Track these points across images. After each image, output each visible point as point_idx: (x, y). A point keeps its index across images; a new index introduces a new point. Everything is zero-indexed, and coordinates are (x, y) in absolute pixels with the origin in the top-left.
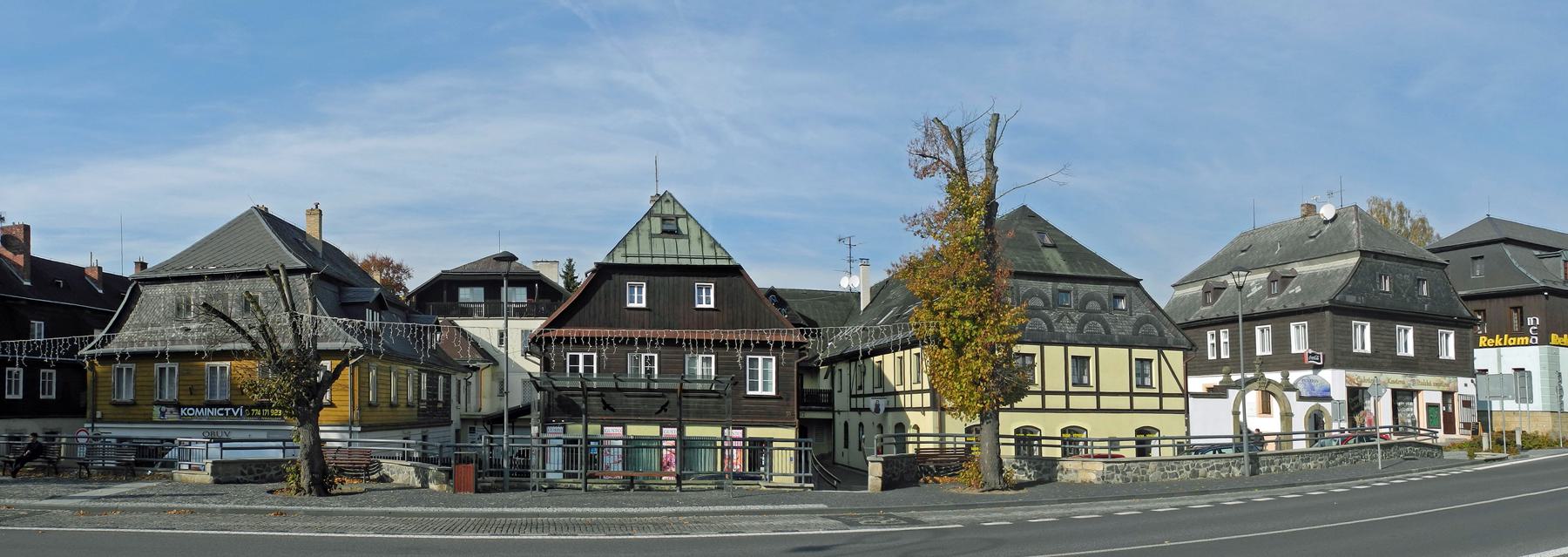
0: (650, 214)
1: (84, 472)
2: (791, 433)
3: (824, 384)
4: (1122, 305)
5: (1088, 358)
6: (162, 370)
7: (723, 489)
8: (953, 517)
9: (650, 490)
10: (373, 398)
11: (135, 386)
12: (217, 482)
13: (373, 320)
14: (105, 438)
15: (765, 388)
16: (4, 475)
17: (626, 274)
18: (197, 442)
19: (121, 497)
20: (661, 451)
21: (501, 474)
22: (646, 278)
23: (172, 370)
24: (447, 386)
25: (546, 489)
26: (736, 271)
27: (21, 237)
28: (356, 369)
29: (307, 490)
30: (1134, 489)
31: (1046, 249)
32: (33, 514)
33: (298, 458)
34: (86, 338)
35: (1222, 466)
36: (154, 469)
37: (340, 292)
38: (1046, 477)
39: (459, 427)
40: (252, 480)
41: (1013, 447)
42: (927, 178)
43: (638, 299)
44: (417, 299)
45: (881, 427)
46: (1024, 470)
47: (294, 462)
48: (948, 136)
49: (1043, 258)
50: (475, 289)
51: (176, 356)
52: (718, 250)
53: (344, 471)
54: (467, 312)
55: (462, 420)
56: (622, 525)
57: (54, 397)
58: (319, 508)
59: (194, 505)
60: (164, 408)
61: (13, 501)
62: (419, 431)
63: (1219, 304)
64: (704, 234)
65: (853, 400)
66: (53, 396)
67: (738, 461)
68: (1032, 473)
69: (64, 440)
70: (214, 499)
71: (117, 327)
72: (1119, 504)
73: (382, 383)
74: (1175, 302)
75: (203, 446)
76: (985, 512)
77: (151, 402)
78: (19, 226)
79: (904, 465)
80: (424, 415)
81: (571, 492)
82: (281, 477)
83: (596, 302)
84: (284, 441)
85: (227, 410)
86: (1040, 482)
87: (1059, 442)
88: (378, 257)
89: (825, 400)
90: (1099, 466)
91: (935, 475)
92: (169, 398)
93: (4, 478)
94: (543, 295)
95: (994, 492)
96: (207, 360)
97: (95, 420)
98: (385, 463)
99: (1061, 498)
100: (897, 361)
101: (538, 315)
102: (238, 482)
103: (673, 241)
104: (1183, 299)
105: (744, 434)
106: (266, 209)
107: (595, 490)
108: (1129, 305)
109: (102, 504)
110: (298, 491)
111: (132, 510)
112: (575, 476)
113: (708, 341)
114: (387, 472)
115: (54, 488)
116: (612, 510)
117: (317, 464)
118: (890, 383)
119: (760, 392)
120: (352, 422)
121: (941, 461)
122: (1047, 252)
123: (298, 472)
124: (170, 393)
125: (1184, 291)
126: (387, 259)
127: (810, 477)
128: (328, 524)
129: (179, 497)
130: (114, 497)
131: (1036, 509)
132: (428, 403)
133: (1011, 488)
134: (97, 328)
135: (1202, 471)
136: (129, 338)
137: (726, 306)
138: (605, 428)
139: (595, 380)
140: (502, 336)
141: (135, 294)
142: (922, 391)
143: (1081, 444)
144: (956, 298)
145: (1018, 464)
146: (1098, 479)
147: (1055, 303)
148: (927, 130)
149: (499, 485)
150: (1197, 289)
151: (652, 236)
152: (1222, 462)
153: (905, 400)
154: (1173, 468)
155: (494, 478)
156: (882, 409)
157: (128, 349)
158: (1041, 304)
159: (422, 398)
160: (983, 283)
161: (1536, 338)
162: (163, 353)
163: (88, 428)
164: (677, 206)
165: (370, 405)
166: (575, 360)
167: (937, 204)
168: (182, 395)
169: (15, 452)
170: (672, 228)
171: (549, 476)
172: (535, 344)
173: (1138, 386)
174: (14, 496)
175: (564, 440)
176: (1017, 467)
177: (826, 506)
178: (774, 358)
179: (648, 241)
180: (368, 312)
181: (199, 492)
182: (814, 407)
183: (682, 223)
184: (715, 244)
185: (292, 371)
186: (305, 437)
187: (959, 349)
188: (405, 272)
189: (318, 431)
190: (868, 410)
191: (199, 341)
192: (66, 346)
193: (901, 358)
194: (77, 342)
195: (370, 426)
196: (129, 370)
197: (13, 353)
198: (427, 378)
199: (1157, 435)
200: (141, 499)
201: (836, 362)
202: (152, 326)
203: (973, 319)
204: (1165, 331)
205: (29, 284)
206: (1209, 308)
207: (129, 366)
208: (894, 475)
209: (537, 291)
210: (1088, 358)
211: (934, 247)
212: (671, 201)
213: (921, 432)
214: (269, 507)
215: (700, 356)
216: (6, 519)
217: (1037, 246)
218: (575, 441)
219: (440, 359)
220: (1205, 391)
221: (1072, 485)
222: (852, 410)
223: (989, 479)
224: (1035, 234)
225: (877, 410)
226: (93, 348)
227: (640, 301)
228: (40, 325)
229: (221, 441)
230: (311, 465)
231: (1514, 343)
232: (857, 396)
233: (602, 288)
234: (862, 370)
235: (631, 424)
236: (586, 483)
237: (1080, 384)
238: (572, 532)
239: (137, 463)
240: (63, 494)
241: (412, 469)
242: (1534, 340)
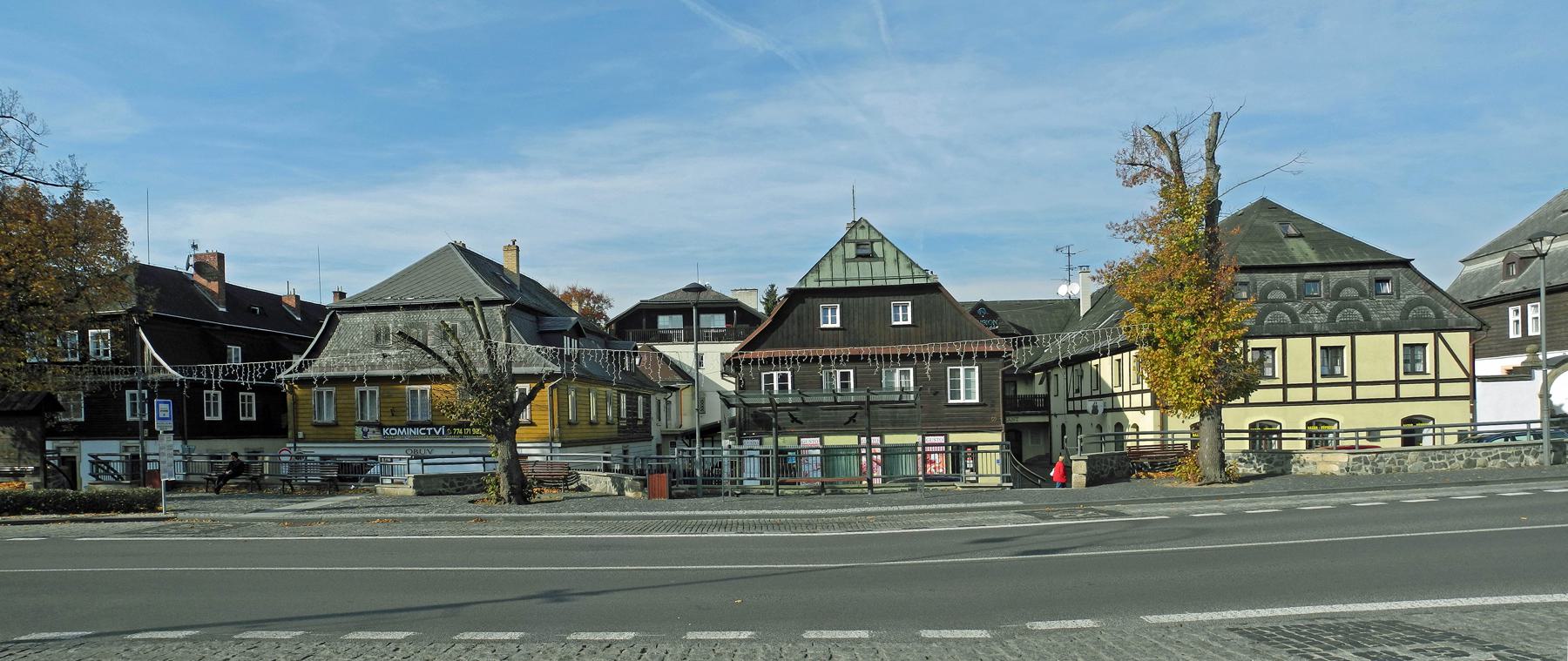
0: (844, 240)
1: (287, 488)
2: (997, 437)
3: (1040, 390)
4: (1387, 288)
5: (1342, 347)
6: (363, 393)
7: (916, 490)
8: (1161, 509)
9: (842, 493)
10: (573, 416)
11: (336, 408)
12: (419, 494)
13: (571, 346)
14: (307, 456)
15: (968, 395)
16: (207, 492)
17: (819, 297)
18: (400, 459)
19: (325, 509)
20: (860, 458)
21: (694, 482)
22: (839, 300)
23: (373, 393)
24: (647, 405)
25: (738, 495)
26: (936, 288)
27: (215, 265)
28: (555, 391)
29: (507, 499)
30: (1380, 481)
31: (1291, 240)
32: (238, 526)
33: (498, 471)
34: (283, 363)
35: (1510, 455)
36: (357, 484)
37: (538, 321)
38: (1278, 469)
39: (659, 443)
40: (454, 492)
41: (1248, 441)
42: (1138, 185)
43: (831, 319)
44: (617, 326)
45: (1100, 427)
46: (1252, 463)
47: (493, 475)
48: (1162, 141)
49: (1286, 250)
50: (674, 317)
51: (373, 380)
52: (915, 270)
54: (666, 338)
55: (663, 436)
56: (807, 525)
57: (255, 419)
58: (518, 515)
59: (397, 515)
60: (366, 429)
61: (217, 515)
62: (620, 446)
63: (1526, 275)
64: (901, 256)
65: (1071, 403)
66: (254, 418)
67: (939, 464)
68: (1262, 467)
69: (267, 459)
70: (416, 509)
71: (316, 352)
72: (1363, 495)
73: (582, 404)
74: (1463, 282)
75: (405, 462)
76: (1162, 507)
77: (353, 423)
78: (213, 254)
79: (1114, 462)
80: (624, 432)
81: (764, 497)
82: (481, 488)
83: (789, 325)
84: (484, 456)
85: (429, 429)
86: (1270, 475)
87: (1303, 435)
88: (579, 289)
89: (1042, 405)
90: (1343, 457)
91: (1150, 471)
92: (371, 418)
93: (208, 494)
94: (740, 321)
95: (1213, 486)
96: (404, 383)
97: (296, 440)
98: (583, 474)
99: (1291, 489)
100: (1116, 364)
101: (736, 339)
102: (440, 494)
103: (867, 264)
104: (1476, 274)
105: (946, 440)
106: (464, 245)
107: (787, 494)
108: (1397, 289)
109: (306, 516)
110: (498, 500)
111: (336, 521)
112: (767, 483)
113: (895, 356)
114: (585, 483)
115: (257, 503)
116: (803, 512)
117: (516, 476)
118: (1107, 385)
119: (962, 400)
120: (553, 439)
121: (1156, 458)
122: (1291, 243)
123: (498, 484)
124: (372, 414)
125: (1478, 265)
126: (588, 291)
127: (1009, 477)
128: (525, 528)
129: (383, 508)
130: (318, 509)
131: (1260, 501)
132: (628, 420)
133: (1234, 481)
134: (297, 354)
135: (1480, 461)
136: (328, 362)
137: (924, 321)
138: (802, 439)
139: (790, 396)
140: (699, 360)
141: (333, 322)
142: (1142, 392)
143: (1331, 436)
144: (1172, 298)
145: (1246, 458)
146: (1342, 471)
147: (1302, 293)
148: (1136, 139)
149: (694, 492)
150: (1497, 261)
151: (846, 261)
152: (1512, 450)
153: (1123, 401)
154: (1440, 458)
155: (688, 486)
156: (1101, 410)
157: (326, 374)
158: (1284, 296)
159: (622, 416)
160: (1203, 282)
162: (360, 378)
163: (290, 448)
164: (872, 231)
165: (570, 423)
166: (769, 378)
168: (385, 416)
169: (218, 470)
170: (868, 252)
171: (746, 483)
172: (731, 365)
173: (1405, 373)
174: (218, 511)
175: (761, 451)
176: (1245, 461)
177: (1021, 503)
178: (977, 368)
179: (842, 266)
180: (566, 339)
181: (401, 503)
182: (1028, 412)
183: (877, 248)
184: (912, 264)
185: (488, 393)
186: (503, 451)
187: (1176, 349)
188: (605, 302)
189: (516, 447)
190: (1086, 412)
191: (396, 366)
192: (262, 370)
193: (1119, 360)
194: (274, 366)
195: (570, 442)
196: (329, 393)
197: (209, 376)
198: (627, 398)
199: (1431, 423)
200: (345, 511)
201: (1052, 368)
202: (351, 352)
203: (1193, 318)
204: (1445, 312)
205: (224, 310)
206: (1513, 280)
207: (329, 389)
208: (1102, 473)
209: (735, 317)
210: (1342, 347)
211: (1147, 251)
212: (867, 227)
213: (1140, 430)
214: (470, 515)
215: (898, 370)
216: (211, 531)
217: (1279, 238)
218: (767, 452)
219: (639, 382)
220: (1504, 373)
221: (1309, 477)
222: (1069, 412)
223: (1208, 473)
224: (1276, 226)
225: (1095, 411)
226: (291, 373)
227: (834, 321)
228: (236, 350)
229: (422, 458)
230: (510, 477)
232: (1073, 399)
233: (795, 311)
234: (1080, 374)
235: (828, 435)
236: (778, 489)
237: (1333, 375)
238: (760, 531)
239: (340, 479)
240: (268, 508)
241: (609, 479)
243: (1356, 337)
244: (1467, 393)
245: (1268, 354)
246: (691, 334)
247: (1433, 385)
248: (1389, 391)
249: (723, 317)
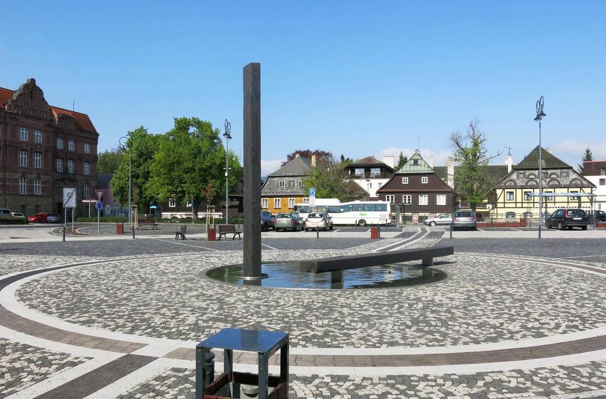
6: (276, 200)
41: (319, 233)
50: (361, 169)
53: (406, 299)
54: (358, 177)
158: (534, 177)
167: (215, 288)
246: (368, 176)
247: (515, 204)
249: (379, 169)
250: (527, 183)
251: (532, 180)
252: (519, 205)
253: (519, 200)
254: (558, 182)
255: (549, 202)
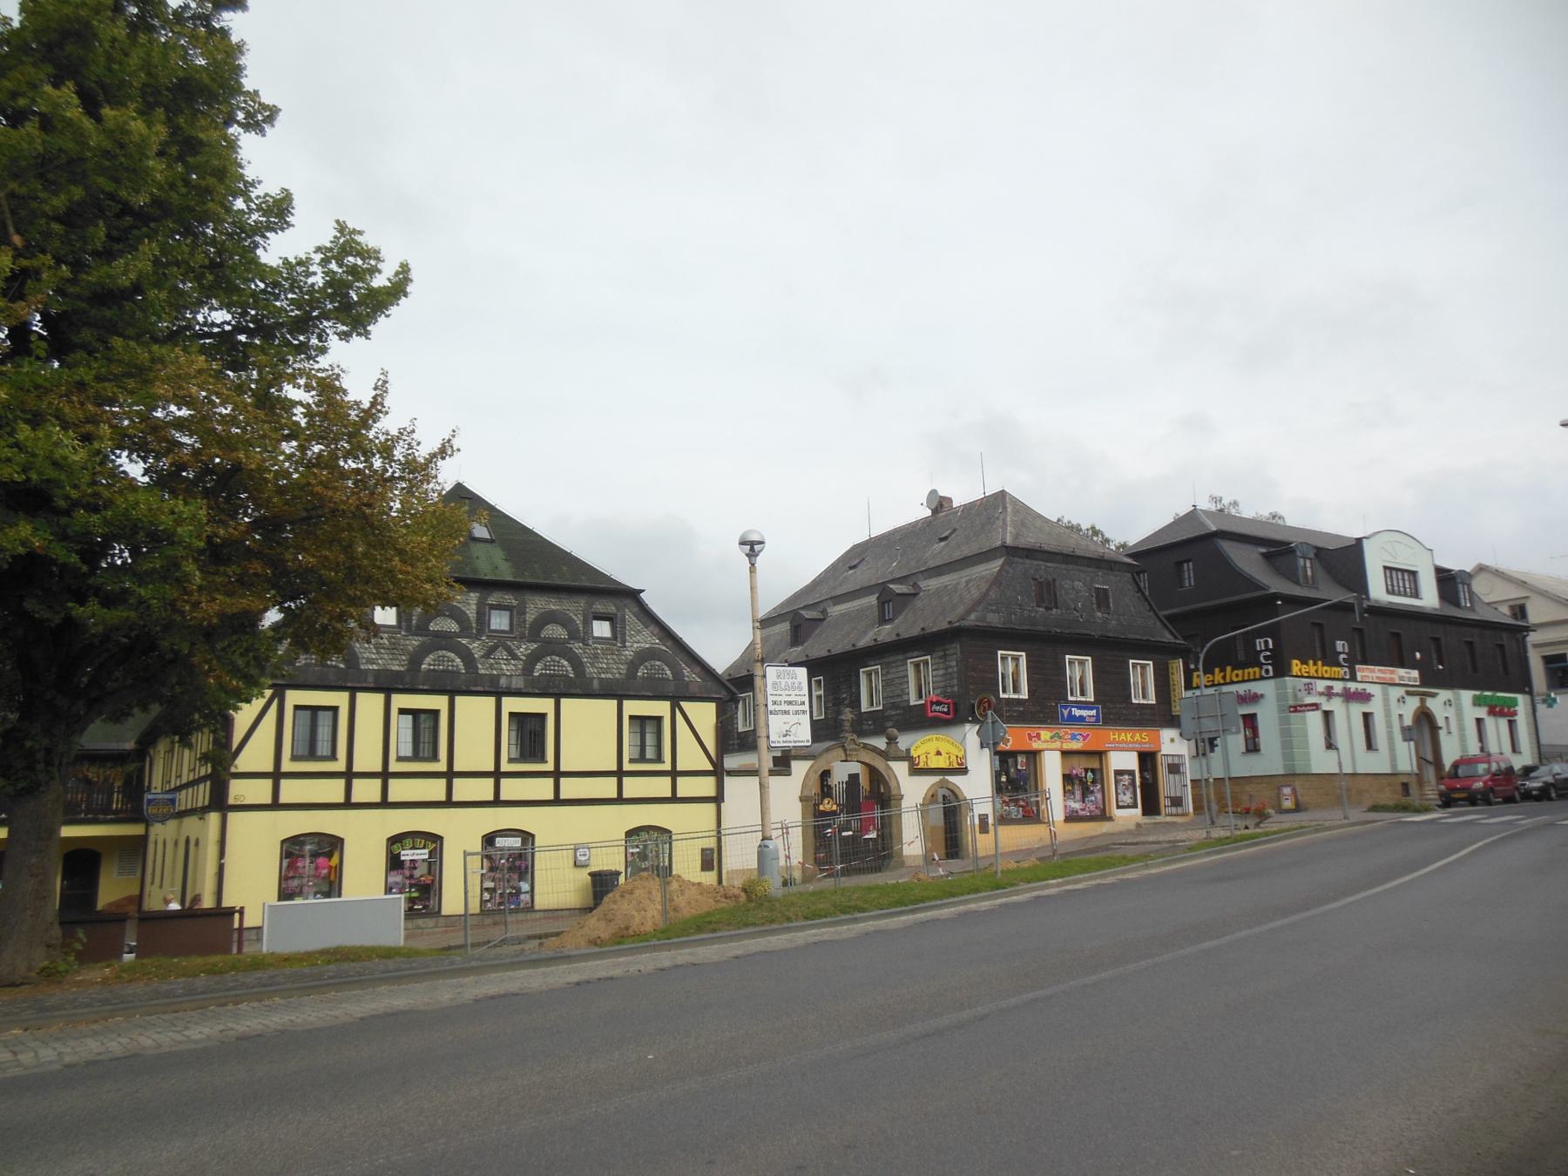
31: (480, 545)
158: (453, 626)
161: (1270, 668)
173: (294, 758)
231: (1240, 679)
237: (312, 755)
242: (1267, 671)
243: (503, 698)
244: (711, 792)
245: (324, 720)
247: (550, 781)
248: (607, 787)
250: (415, 660)
251: (443, 641)
252: (366, 790)
253: (368, 757)
254: (576, 663)
255: (1201, 765)
